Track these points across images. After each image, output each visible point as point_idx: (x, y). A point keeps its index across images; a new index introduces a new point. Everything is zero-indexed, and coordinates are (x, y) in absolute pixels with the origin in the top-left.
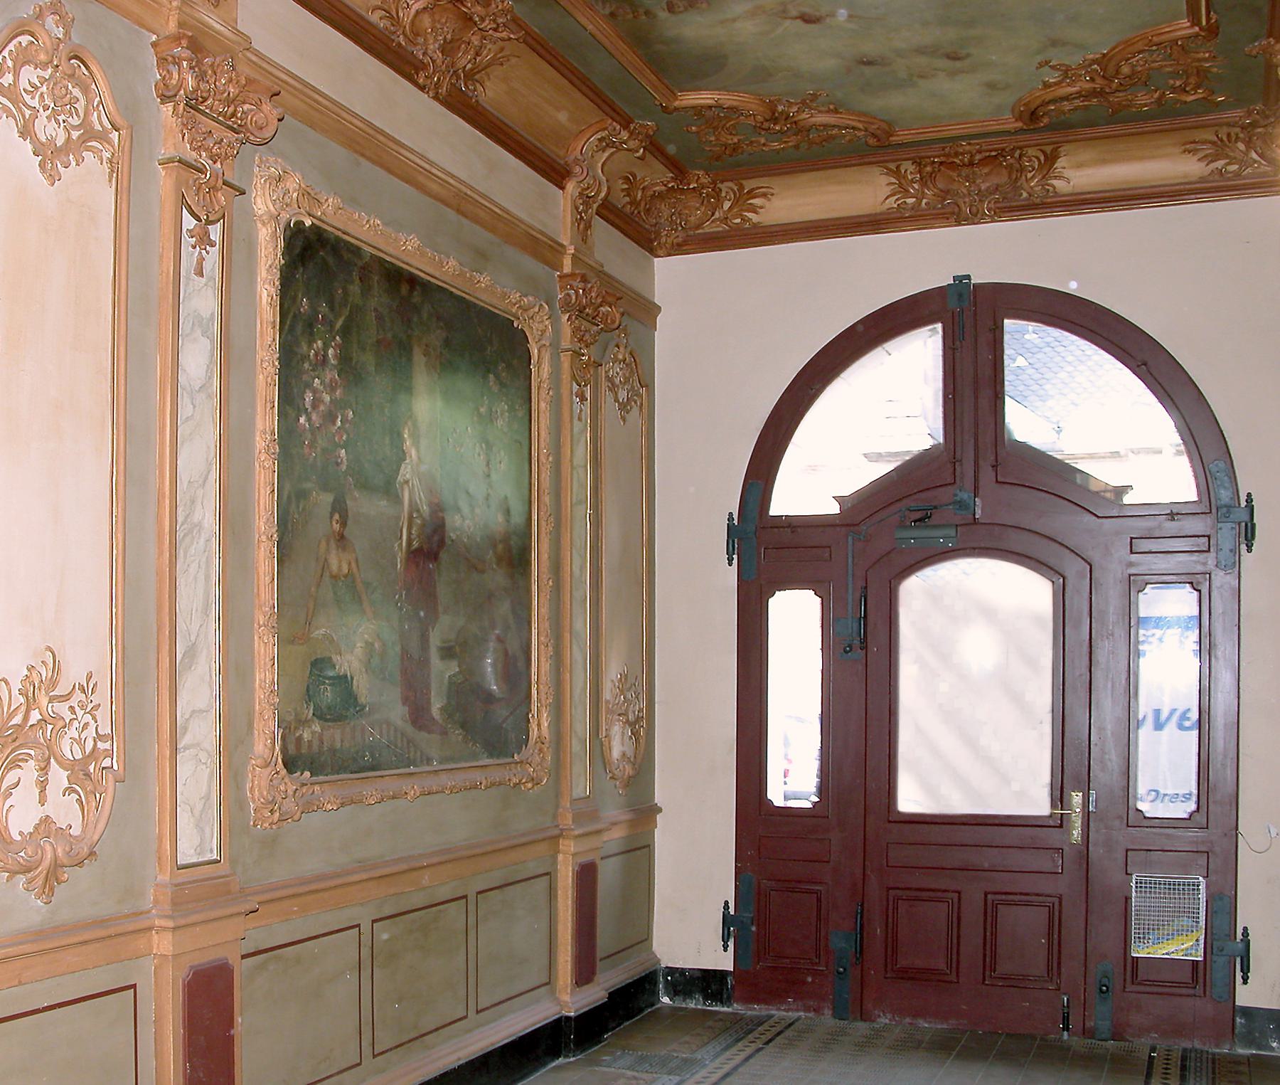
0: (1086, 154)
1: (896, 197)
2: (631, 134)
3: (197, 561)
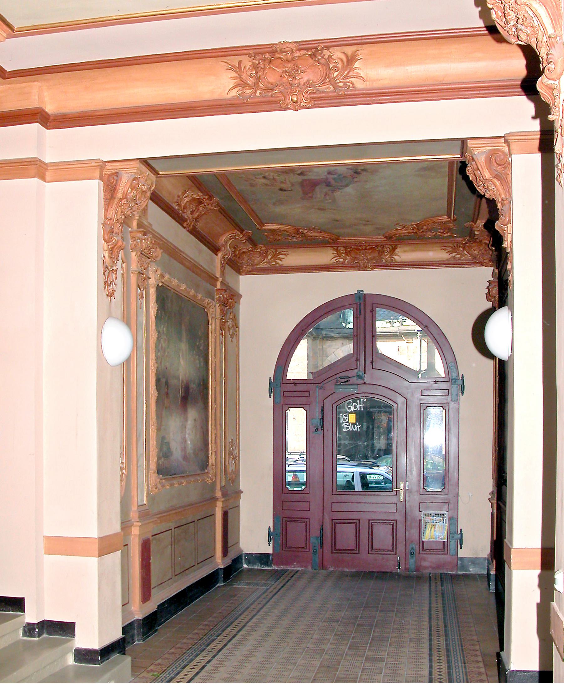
0: (407, 248)
2: (244, 236)
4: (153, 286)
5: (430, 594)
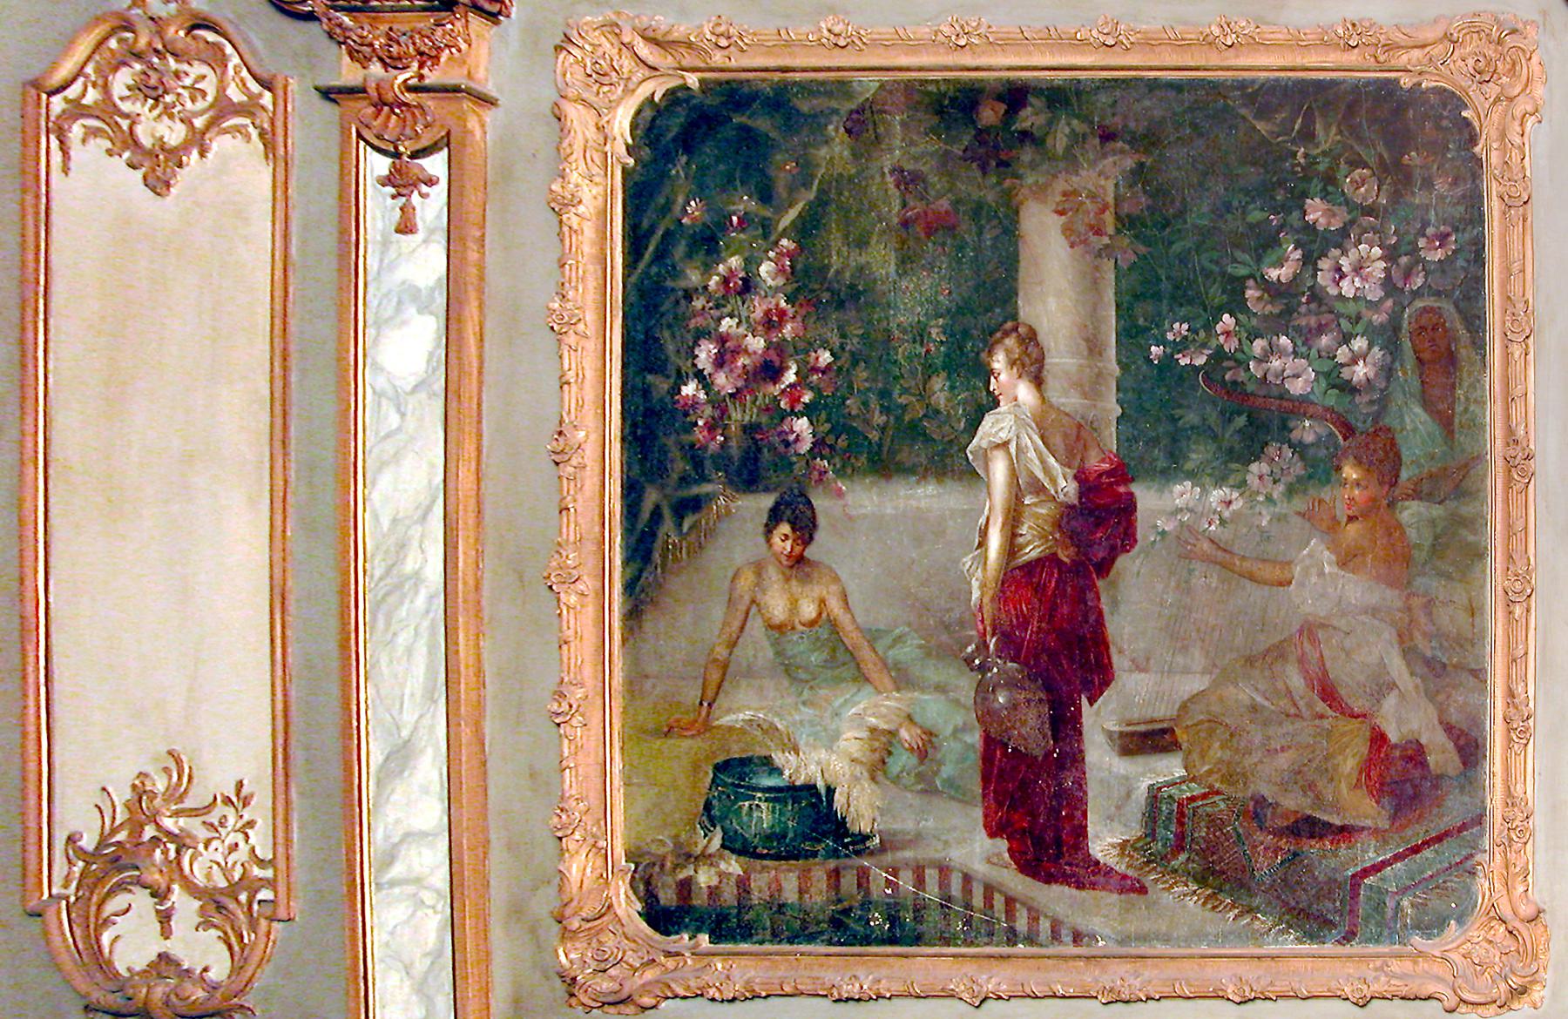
3: (412, 627)
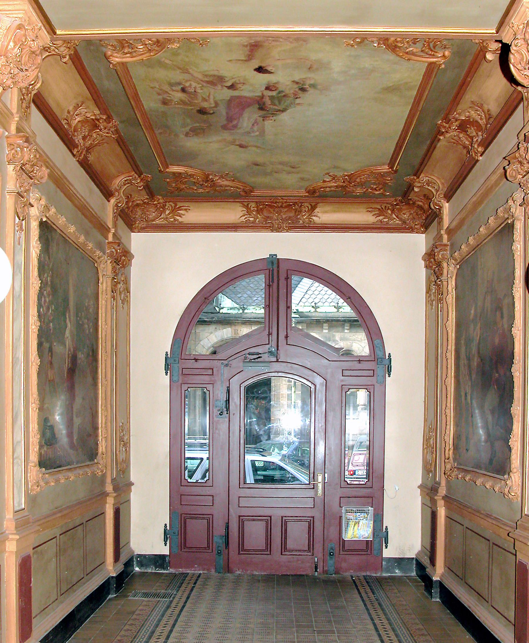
0: (327, 208)
1: (245, 217)
4: (35, 218)
5: (365, 605)
